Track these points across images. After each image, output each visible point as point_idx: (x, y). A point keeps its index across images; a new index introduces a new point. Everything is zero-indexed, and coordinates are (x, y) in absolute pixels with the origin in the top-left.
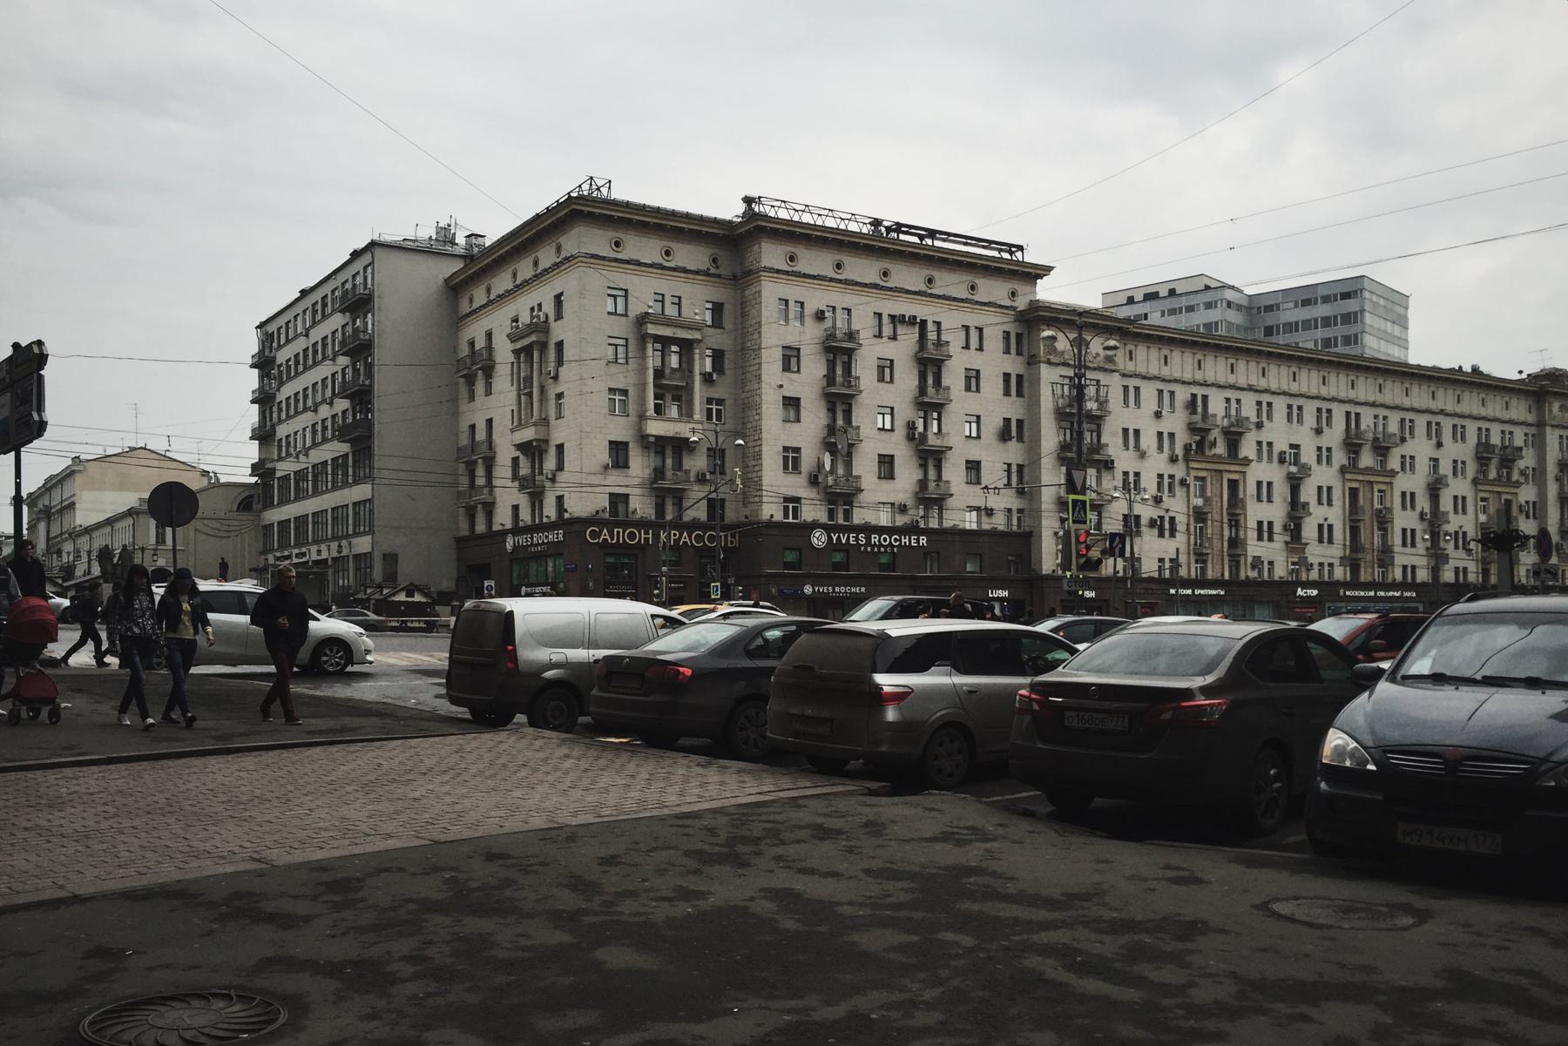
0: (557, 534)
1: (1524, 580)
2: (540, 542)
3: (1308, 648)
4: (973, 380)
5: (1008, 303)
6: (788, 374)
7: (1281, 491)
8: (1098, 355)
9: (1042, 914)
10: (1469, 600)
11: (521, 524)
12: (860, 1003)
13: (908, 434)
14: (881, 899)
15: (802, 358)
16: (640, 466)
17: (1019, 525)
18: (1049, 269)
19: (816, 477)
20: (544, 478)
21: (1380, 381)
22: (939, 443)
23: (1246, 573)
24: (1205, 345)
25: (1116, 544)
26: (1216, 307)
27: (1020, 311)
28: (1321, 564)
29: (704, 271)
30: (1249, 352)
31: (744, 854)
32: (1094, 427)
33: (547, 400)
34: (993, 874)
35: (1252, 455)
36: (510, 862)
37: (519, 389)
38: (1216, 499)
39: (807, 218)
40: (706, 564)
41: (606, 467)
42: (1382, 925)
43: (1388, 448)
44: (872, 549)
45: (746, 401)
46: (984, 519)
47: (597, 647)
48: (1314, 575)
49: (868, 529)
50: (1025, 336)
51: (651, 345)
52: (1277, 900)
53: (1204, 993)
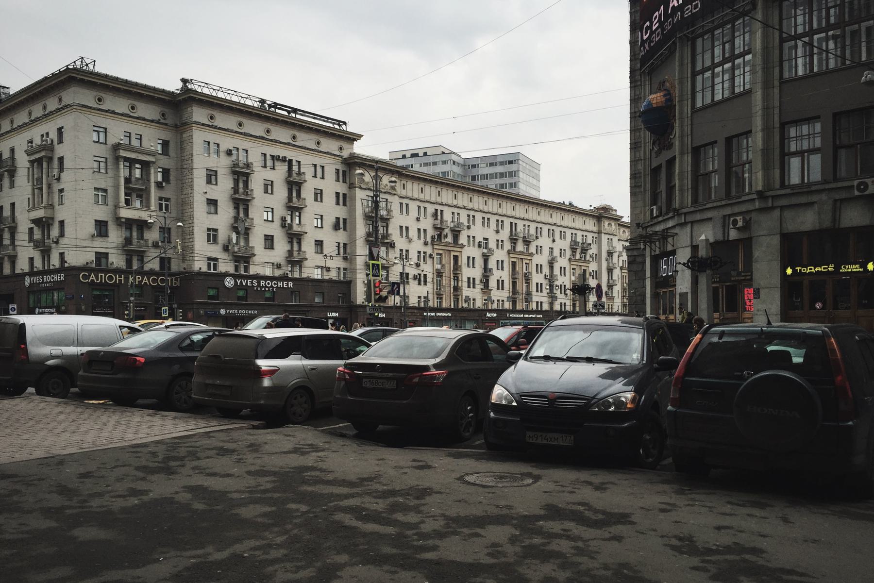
0: (60, 276)
1: (591, 310)
3: (487, 344)
4: (319, 195)
5: (338, 153)
6: (210, 186)
7: (479, 262)
8: (387, 185)
9: (345, 490)
10: (562, 319)
11: (35, 270)
12: (238, 548)
13: (282, 223)
14: (256, 487)
15: (218, 176)
16: (115, 236)
17: (344, 277)
18: (360, 136)
19: (227, 246)
20: (51, 241)
21: (526, 207)
22: (299, 229)
23: (462, 304)
24: (442, 183)
25: (394, 288)
26: (447, 163)
28: (498, 301)
29: (156, 120)
30: (464, 188)
31: (174, 466)
32: (384, 224)
33: (52, 192)
34: (321, 470)
35: (465, 243)
36: (16, 480)
37: (33, 185)
38: (447, 266)
39: (220, 95)
40: (159, 296)
41: (93, 236)
42: (516, 484)
43: (530, 242)
44: (261, 289)
45: (184, 200)
46: (325, 273)
47: (83, 345)
48: (495, 306)
49: (259, 277)
50: (347, 173)
51: (122, 163)
52: (467, 474)
53: (428, 526)
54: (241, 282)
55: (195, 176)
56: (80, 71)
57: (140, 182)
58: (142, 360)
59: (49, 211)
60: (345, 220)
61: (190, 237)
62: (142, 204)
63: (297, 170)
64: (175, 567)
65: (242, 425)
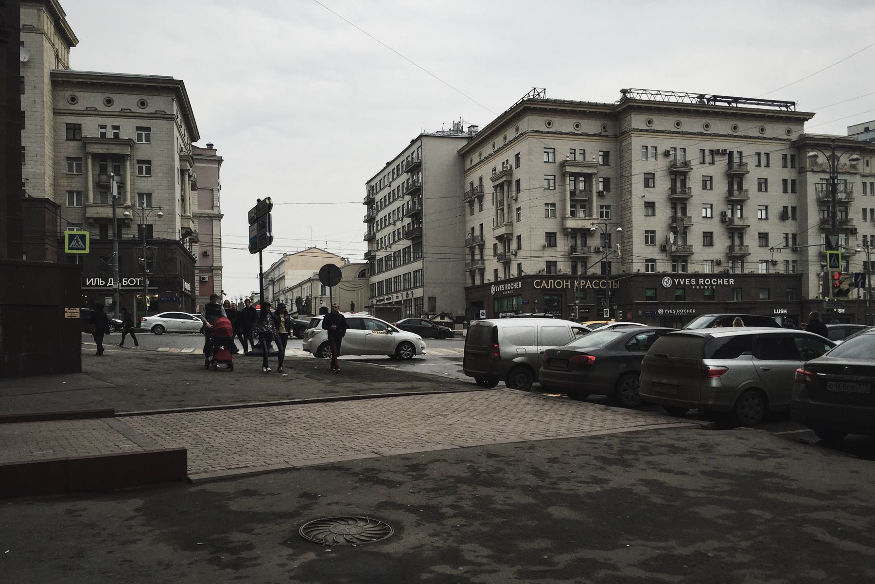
0: (518, 284)
4: (763, 184)
5: (785, 137)
9: (813, 502)
11: (499, 279)
12: (701, 546)
15: (656, 179)
16: (563, 245)
17: (794, 270)
18: (813, 114)
19: (665, 247)
20: (511, 254)
22: (741, 223)
32: (843, 209)
33: (511, 212)
36: (499, 459)
37: (497, 207)
39: (659, 98)
40: (601, 298)
41: (544, 247)
44: (700, 287)
46: (771, 267)
49: (697, 276)
54: (679, 281)
55: (633, 181)
56: (533, 101)
57: (584, 193)
58: (594, 358)
59: (510, 228)
60: (794, 209)
61: (629, 240)
62: (586, 214)
63: (739, 161)
64: (642, 555)
65: (687, 425)
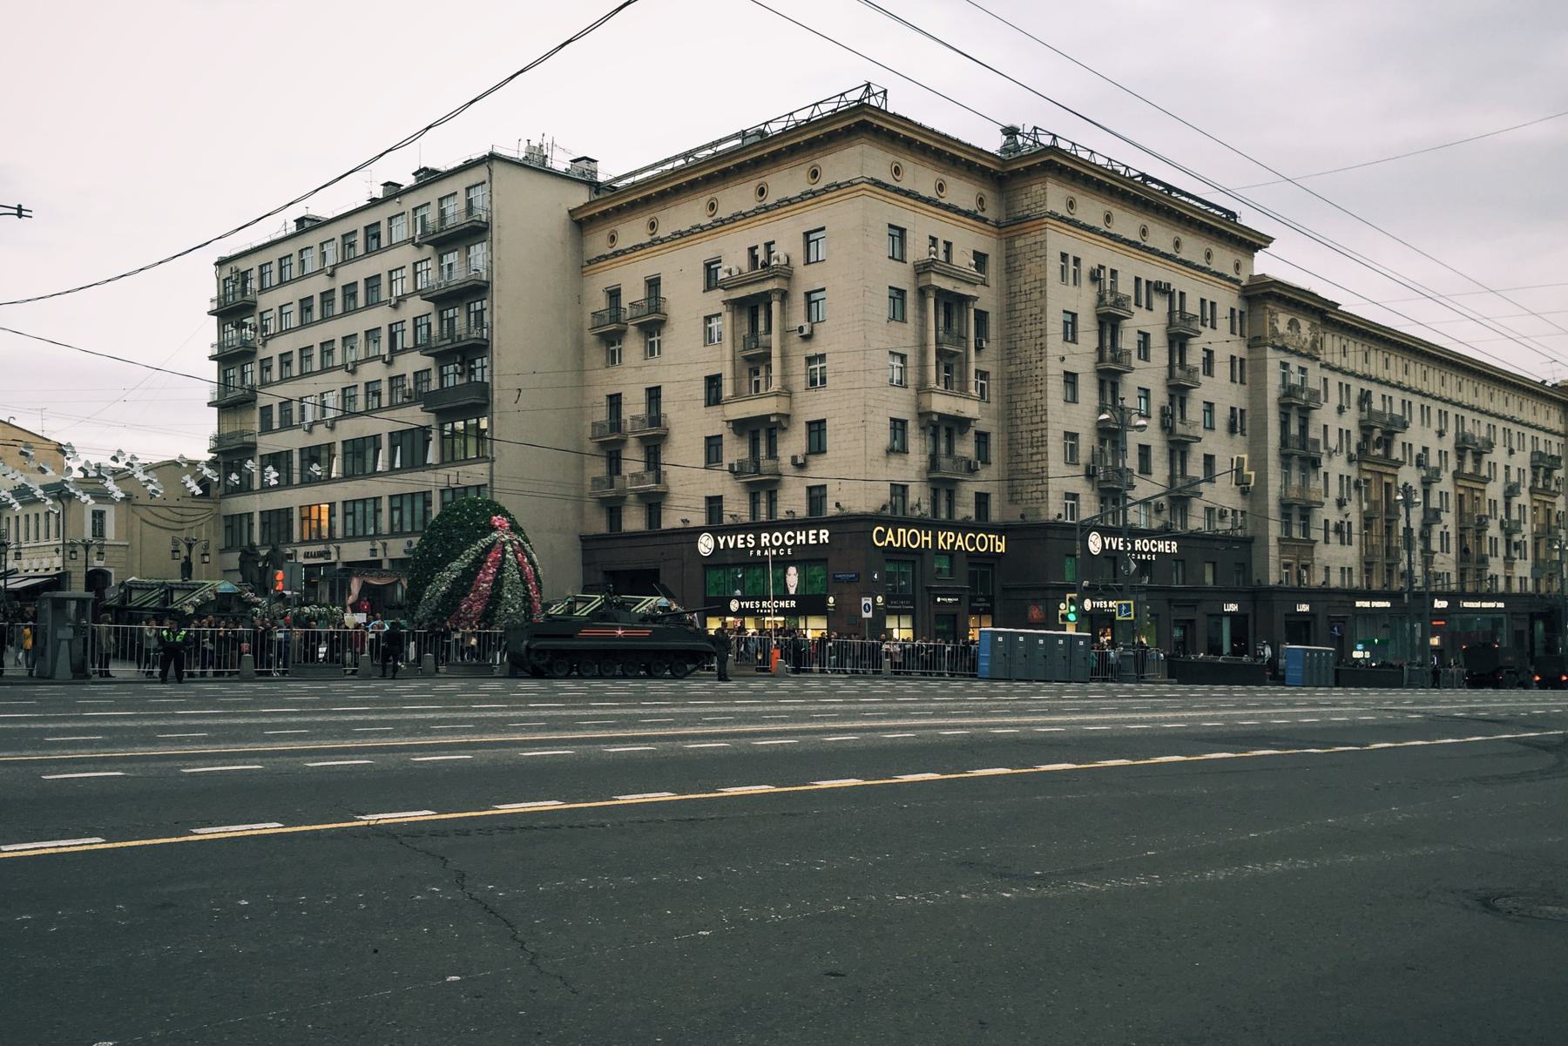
2: (1146, 550)
5: (1231, 274)
16: (917, 446)
27: (1244, 287)
44: (786, 552)
50: (1246, 314)
